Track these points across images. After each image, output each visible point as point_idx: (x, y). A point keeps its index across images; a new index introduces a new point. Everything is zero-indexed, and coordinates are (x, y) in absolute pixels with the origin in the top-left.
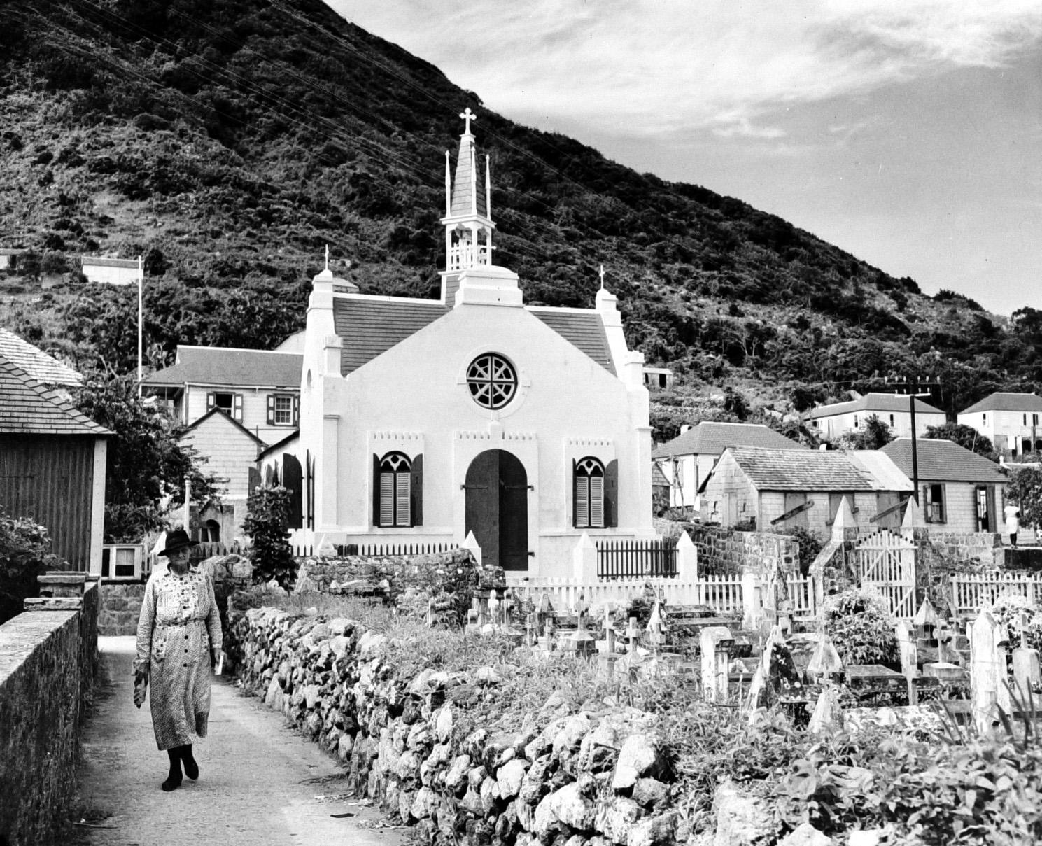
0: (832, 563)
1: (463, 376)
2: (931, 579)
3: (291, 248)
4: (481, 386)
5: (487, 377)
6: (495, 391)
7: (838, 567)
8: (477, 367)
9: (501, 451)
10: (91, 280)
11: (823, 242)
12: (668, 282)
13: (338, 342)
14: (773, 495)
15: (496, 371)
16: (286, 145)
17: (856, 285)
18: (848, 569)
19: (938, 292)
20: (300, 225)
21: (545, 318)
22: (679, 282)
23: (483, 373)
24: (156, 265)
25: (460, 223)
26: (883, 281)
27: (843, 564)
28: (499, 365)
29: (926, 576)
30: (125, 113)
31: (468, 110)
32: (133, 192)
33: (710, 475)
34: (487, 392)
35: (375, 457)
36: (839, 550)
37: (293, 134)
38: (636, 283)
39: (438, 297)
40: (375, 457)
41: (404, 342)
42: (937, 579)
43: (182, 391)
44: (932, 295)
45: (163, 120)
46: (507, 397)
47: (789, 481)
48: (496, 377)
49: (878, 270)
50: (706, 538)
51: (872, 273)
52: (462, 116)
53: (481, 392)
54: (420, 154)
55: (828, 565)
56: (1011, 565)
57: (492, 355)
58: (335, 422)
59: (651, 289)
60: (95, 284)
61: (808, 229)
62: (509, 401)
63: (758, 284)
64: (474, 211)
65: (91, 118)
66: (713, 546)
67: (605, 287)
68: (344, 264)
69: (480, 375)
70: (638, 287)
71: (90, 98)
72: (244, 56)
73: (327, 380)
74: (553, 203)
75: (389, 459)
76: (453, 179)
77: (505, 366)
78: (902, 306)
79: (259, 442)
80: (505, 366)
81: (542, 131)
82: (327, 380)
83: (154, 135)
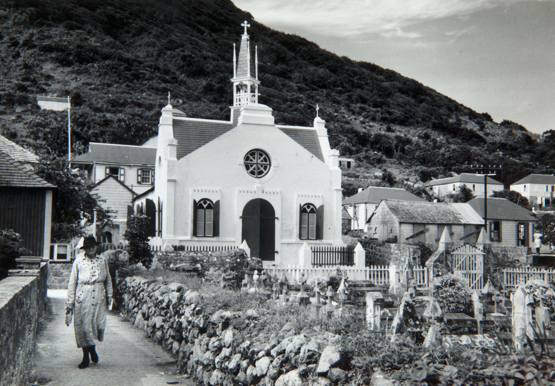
1: (242, 161)
2: (492, 270)
4: (252, 166)
6: (259, 169)
7: (441, 262)
8: (250, 156)
12: (354, 113)
13: (175, 142)
15: (260, 158)
19: (502, 121)
21: (286, 131)
22: (359, 114)
23: (253, 159)
25: (241, 81)
27: (444, 261)
31: (246, 22)
32: (64, 62)
33: (373, 214)
34: (254, 169)
35: (195, 201)
36: (442, 254)
38: (336, 114)
40: (195, 201)
47: (416, 218)
48: (259, 161)
50: (370, 246)
51: (466, 110)
52: (242, 25)
53: (251, 169)
55: (436, 261)
58: (173, 183)
59: (344, 117)
60: (45, 110)
62: (266, 174)
64: (249, 75)
66: (374, 251)
67: (319, 116)
68: (178, 102)
69: (251, 160)
77: (264, 156)
82: (169, 162)
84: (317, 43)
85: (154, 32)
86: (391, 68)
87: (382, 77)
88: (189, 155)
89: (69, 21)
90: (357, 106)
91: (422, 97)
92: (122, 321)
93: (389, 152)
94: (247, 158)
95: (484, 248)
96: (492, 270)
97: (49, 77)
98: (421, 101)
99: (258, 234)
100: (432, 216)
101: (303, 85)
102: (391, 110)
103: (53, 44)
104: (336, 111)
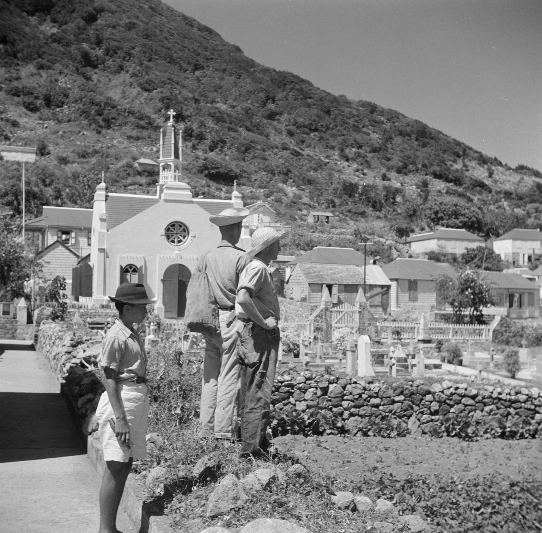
0: (318, 316)
1: (163, 232)
2: (367, 324)
3: (122, 140)
5: (175, 232)
7: (321, 317)
9: (180, 265)
10: (5, 159)
11: (446, 136)
12: (347, 160)
14: (316, 286)
16: (124, 77)
17: (463, 162)
18: (326, 319)
19: (517, 165)
20: (128, 127)
22: (354, 160)
24: (42, 151)
26: (483, 160)
27: (324, 317)
28: (180, 226)
29: (364, 323)
30: (28, 59)
31: (172, 110)
32: (32, 108)
33: (291, 276)
35: (121, 267)
36: (322, 311)
37: (127, 72)
38: (327, 161)
39: (155, 195)
40: (121, 267)
41: (138, 215)
42: (370, 324)
43: (45, 231)
44: (514, 166)
45: (49, 64)
46: (184, 240)
47: (325, 279)
48: (179, 232)
49: (480, 153)
51: (476, 155)
52: (169, 113)
54: (203, 84)
55: (316, 317)
56: (438, 320)
57: (177, 222)
59: (336, 164)
60: (7, 162)
61: (438, 128)
63: (401, 162)
64: (173, 157)
65: (7, 63)
68: (152, 150)
70: (328, 163)
71: (6, 51)
72: (98, 25)
73: (100, 233)
74: (281, 114)
75: (128, 267)
76: (164, 142)
77: (183, 227)
78: (491, 175)
79: (78, 256)
80: (183, 227)
81: (278, 70)
82: (100, 233)
83: (44, 73)
84: (311, 81)
85: (131, 70)
86: (393, 108)
87: (382, 118)
88: (118, 227)
89: (40, 60)
90: (351, 152)
91: (427, 140)
92: (224, 526)
93: (376, 206)
94: (168, 229)
95: (361, 306)
96: (367, 324)
97: (15, 124)
98: (424, 145)
99: (177, 294)
100: (342, 277)
101: (293, 128)
102: (389, 156)
103: (21, 87)
104: (328, 157)
